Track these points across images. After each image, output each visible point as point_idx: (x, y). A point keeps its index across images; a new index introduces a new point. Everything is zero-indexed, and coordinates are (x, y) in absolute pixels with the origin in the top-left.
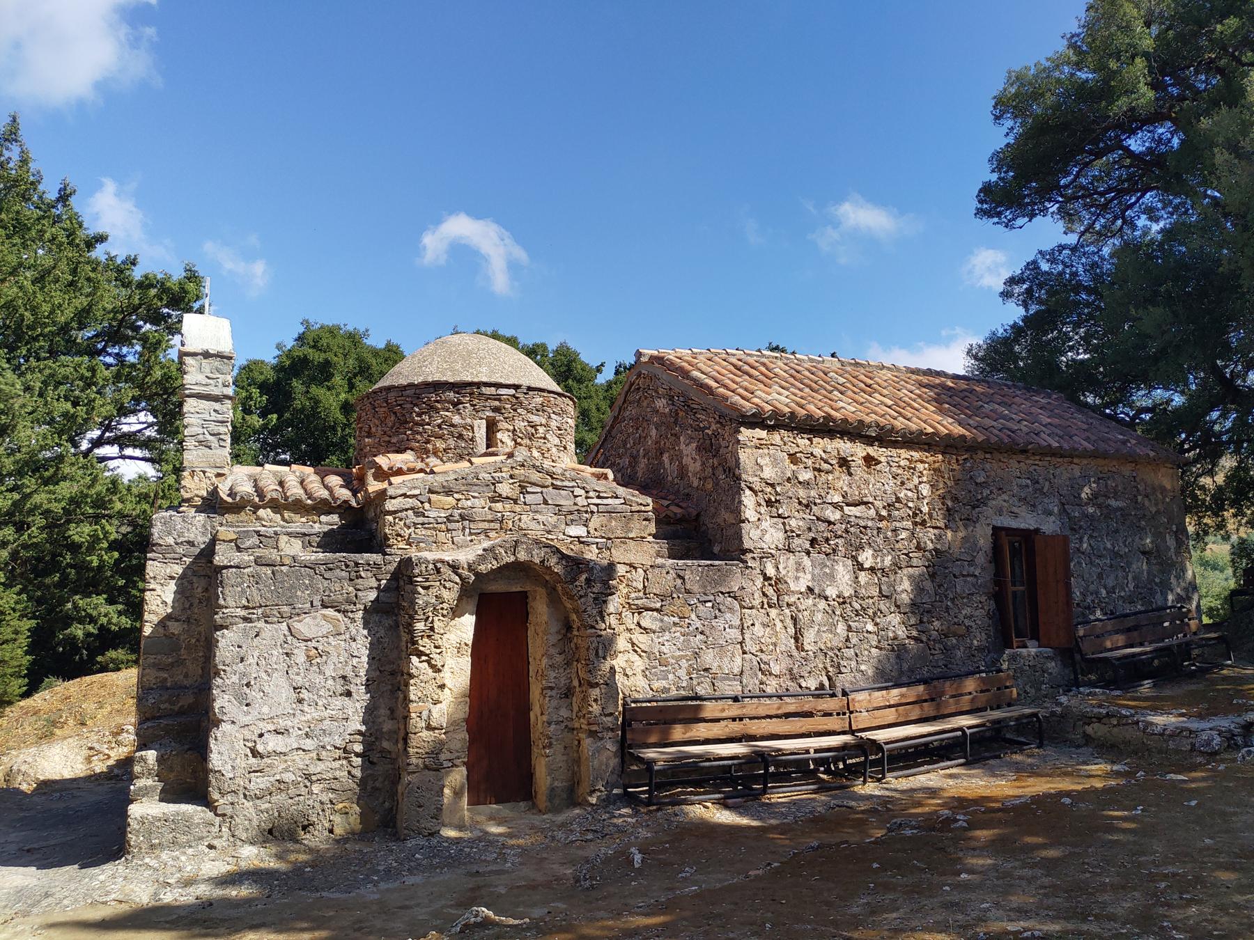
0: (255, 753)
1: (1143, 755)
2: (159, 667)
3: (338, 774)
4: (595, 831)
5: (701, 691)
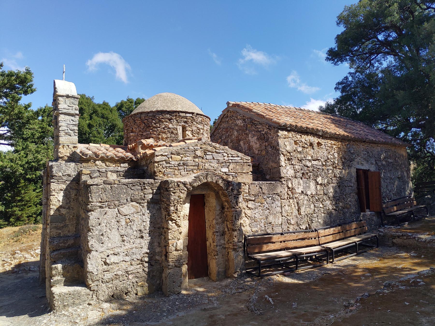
0: (106, 263)
1: (417, 250)
2: (57, 228)
3: (139, 270)
5: (269, 231)
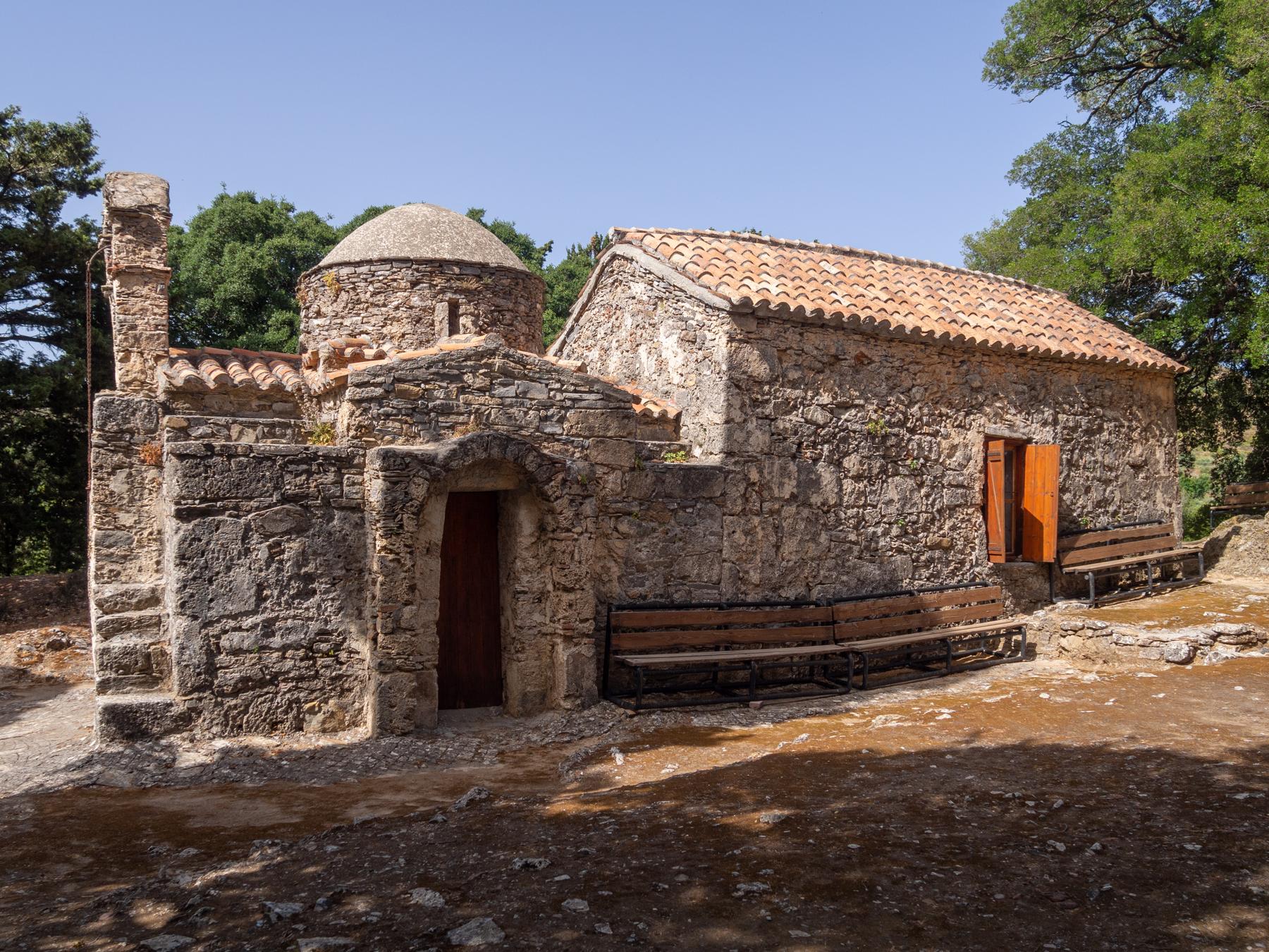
4: (572, 734)
